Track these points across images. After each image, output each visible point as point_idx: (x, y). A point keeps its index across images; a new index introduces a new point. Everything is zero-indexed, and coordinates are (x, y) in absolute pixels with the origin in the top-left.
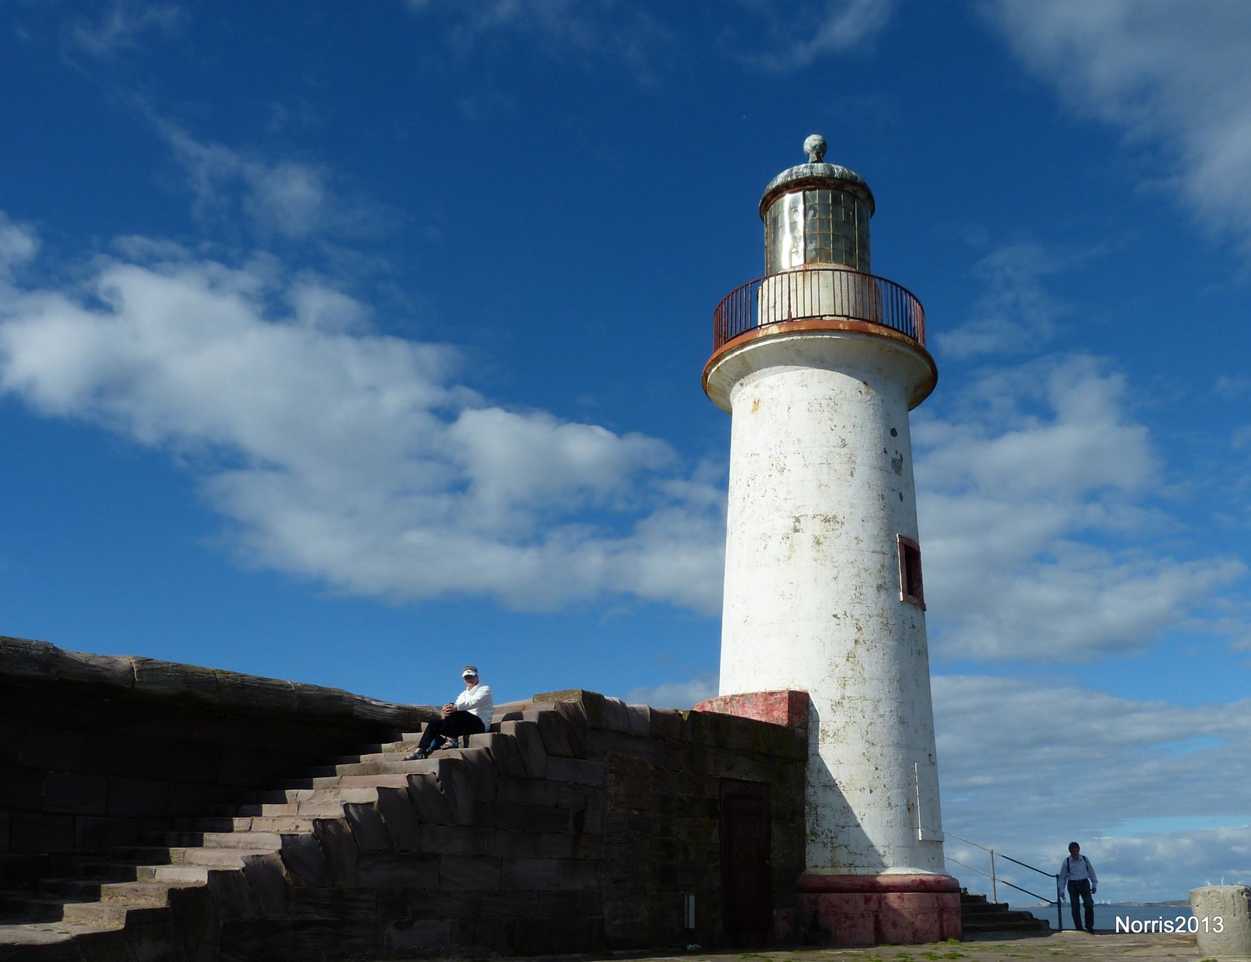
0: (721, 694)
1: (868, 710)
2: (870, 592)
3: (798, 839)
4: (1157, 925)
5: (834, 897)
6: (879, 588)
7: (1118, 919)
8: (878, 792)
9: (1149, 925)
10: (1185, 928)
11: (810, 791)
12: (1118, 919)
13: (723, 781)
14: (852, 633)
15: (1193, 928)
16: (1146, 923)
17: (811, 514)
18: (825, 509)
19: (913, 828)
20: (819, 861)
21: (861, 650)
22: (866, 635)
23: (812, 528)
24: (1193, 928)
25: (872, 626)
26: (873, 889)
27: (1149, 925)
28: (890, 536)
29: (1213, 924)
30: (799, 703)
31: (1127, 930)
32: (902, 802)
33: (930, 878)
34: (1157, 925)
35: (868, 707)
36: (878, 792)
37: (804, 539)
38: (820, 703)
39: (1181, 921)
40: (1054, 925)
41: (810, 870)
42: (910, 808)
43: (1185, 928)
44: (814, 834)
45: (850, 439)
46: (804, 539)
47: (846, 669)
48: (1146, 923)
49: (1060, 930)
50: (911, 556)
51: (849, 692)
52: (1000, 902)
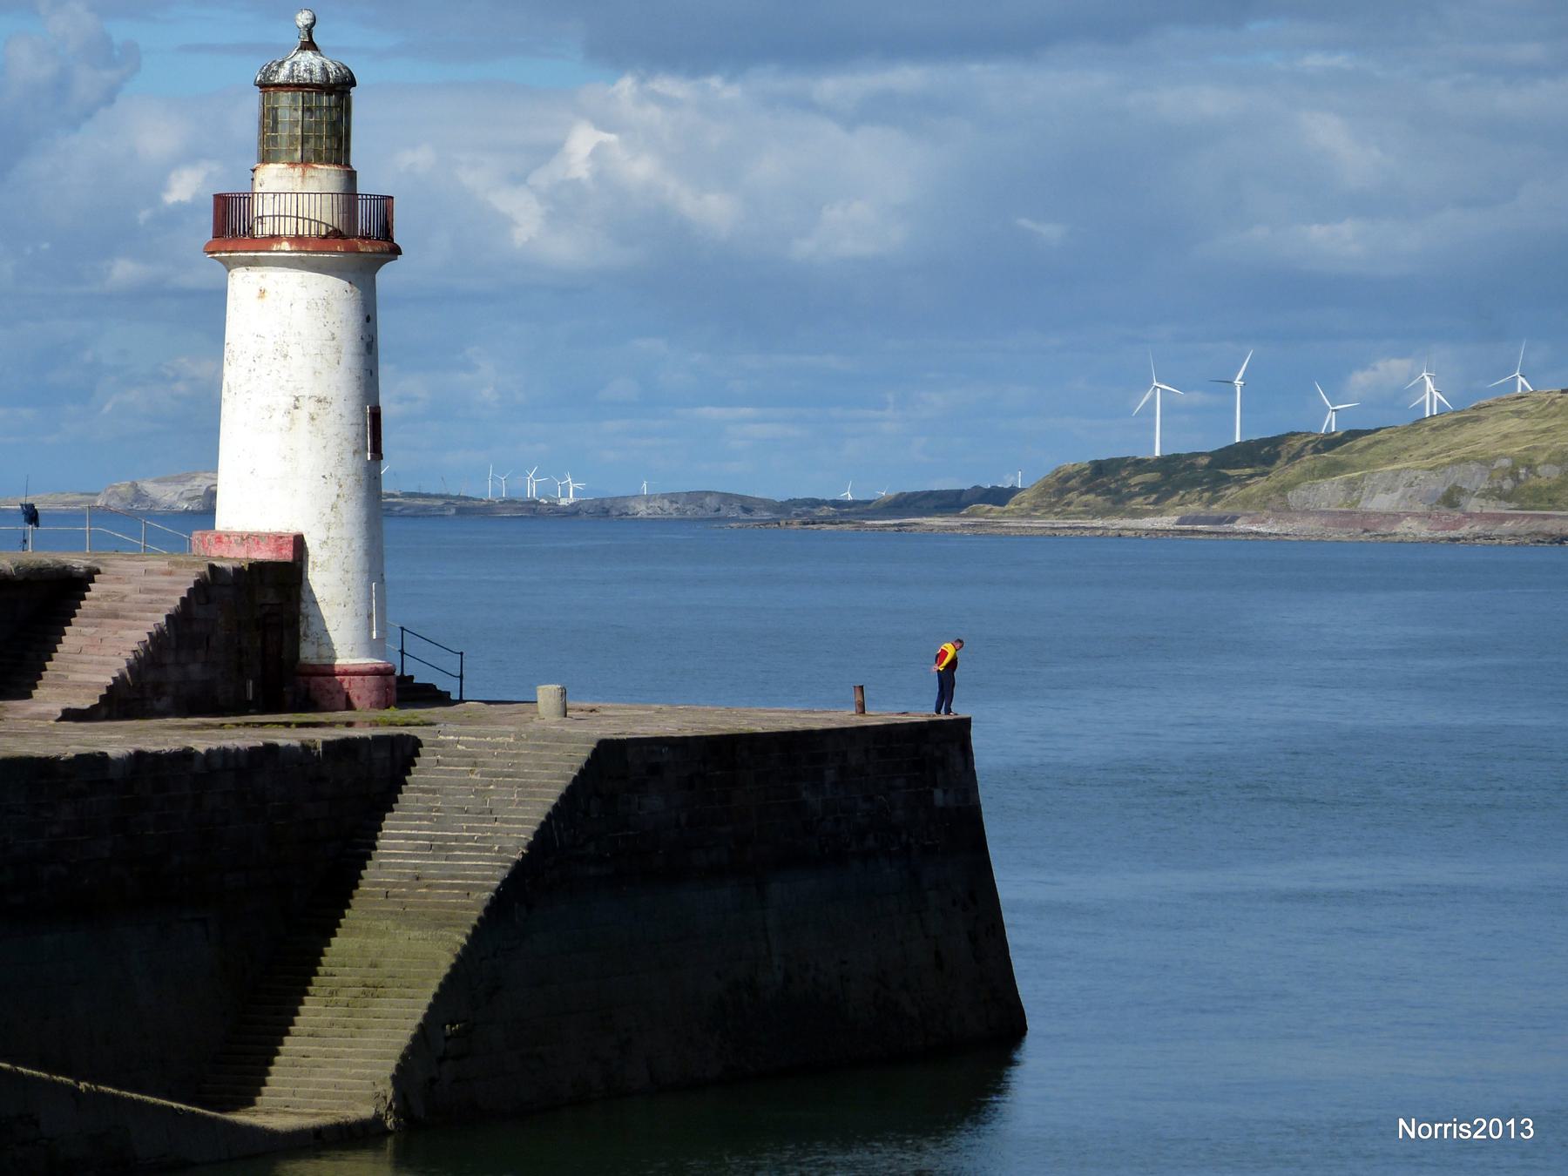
0: (218, 527)
1: (345, 547)
2: (349, 456)
3: (296, 639)
4: (1451, 1129)
5: (321, 679)
6: (355, 452)
7: (1402, 1122)
8: (349, 606)
9: (1441, 1129)
10: (1486, 1132)
11: (303, 605)
12: (1402, 1122)
13: (262, 605)
14: (335, 489)
15: (1496, 1133)
16: (1437, 1126)
17: (307, 394)
18: (319, 392)
19: (371, 631)
20: (308, 653)
21: (341, 502)
22: (345, 490)
23: (308, 407)
24: (1496, 1133)
25: (349, 482)
26: (328, 671)
27: (1441, 1129)
28: (364, 409)
29: (1520, 1128)
30: (299, 542)
31: (1412, 1135)
32: (364, 612)
33: (323, 639)
34: (1451, 1129)
35: (345, 544)
36: (349, 606)
37: (302, 415)
38: (311, 543)
39: (1480, 1124)
40: (455, 696)
41: (302, 656)
42: (370, 616)
43: (1486, 1132)
44: (306, 635)
45: (338, 333)
46: (302, 415)
47: (330, 516)
48: (1437, 1126)
49: (461, 701)
50: (376, 416)
51: (332, 534)
52: (406, 674)
